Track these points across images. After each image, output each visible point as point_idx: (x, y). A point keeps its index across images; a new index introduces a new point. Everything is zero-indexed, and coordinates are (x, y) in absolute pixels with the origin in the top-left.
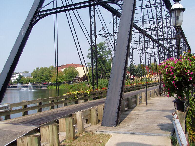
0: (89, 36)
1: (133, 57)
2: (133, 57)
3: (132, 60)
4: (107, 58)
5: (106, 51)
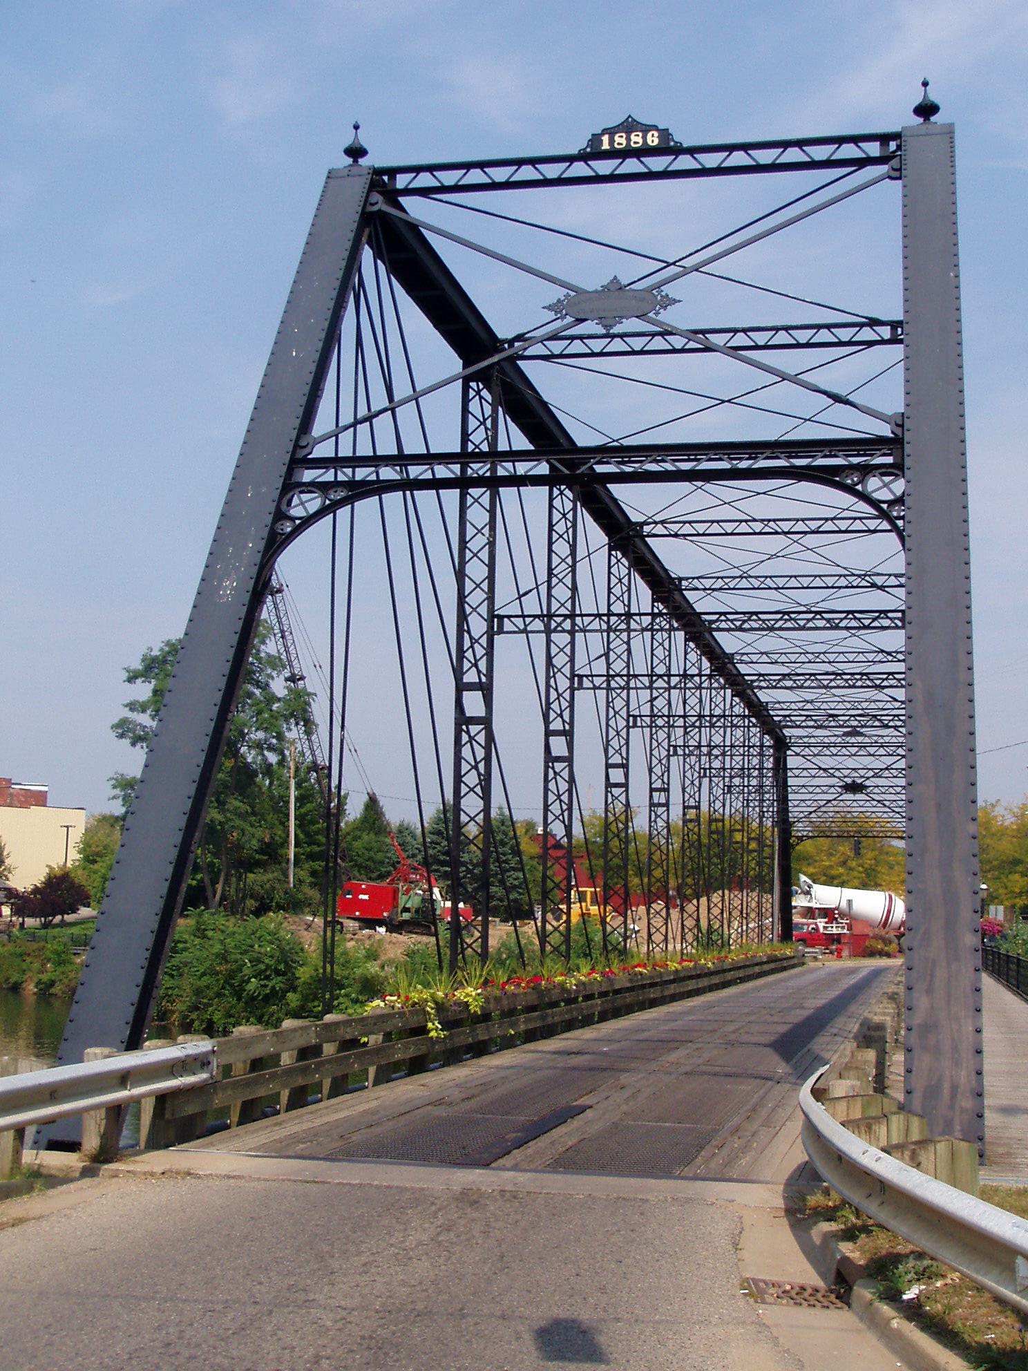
0: (863, 349)
1: (570, 746)
2: (570, 746)
3: (481, 738)
4: (271, 748)
5: (272, 699)
